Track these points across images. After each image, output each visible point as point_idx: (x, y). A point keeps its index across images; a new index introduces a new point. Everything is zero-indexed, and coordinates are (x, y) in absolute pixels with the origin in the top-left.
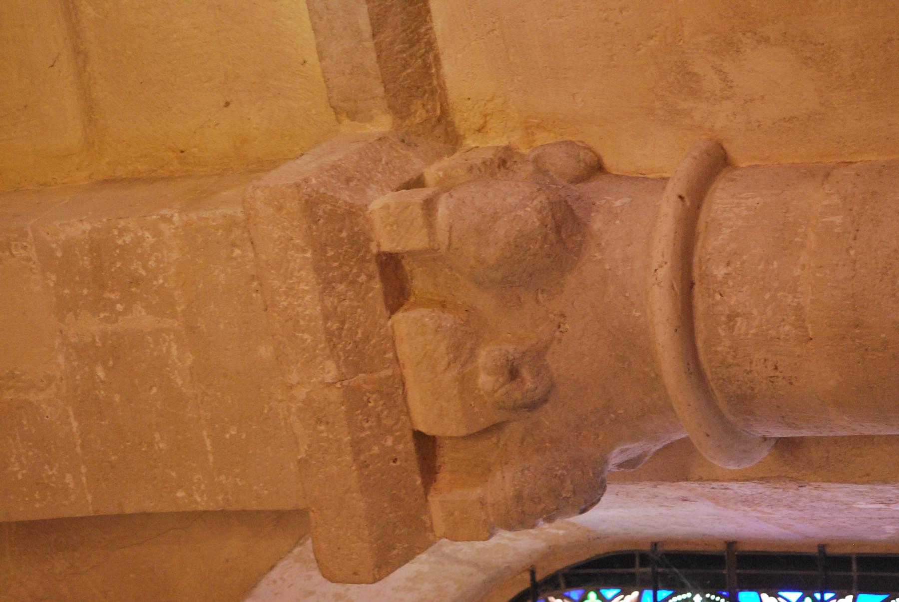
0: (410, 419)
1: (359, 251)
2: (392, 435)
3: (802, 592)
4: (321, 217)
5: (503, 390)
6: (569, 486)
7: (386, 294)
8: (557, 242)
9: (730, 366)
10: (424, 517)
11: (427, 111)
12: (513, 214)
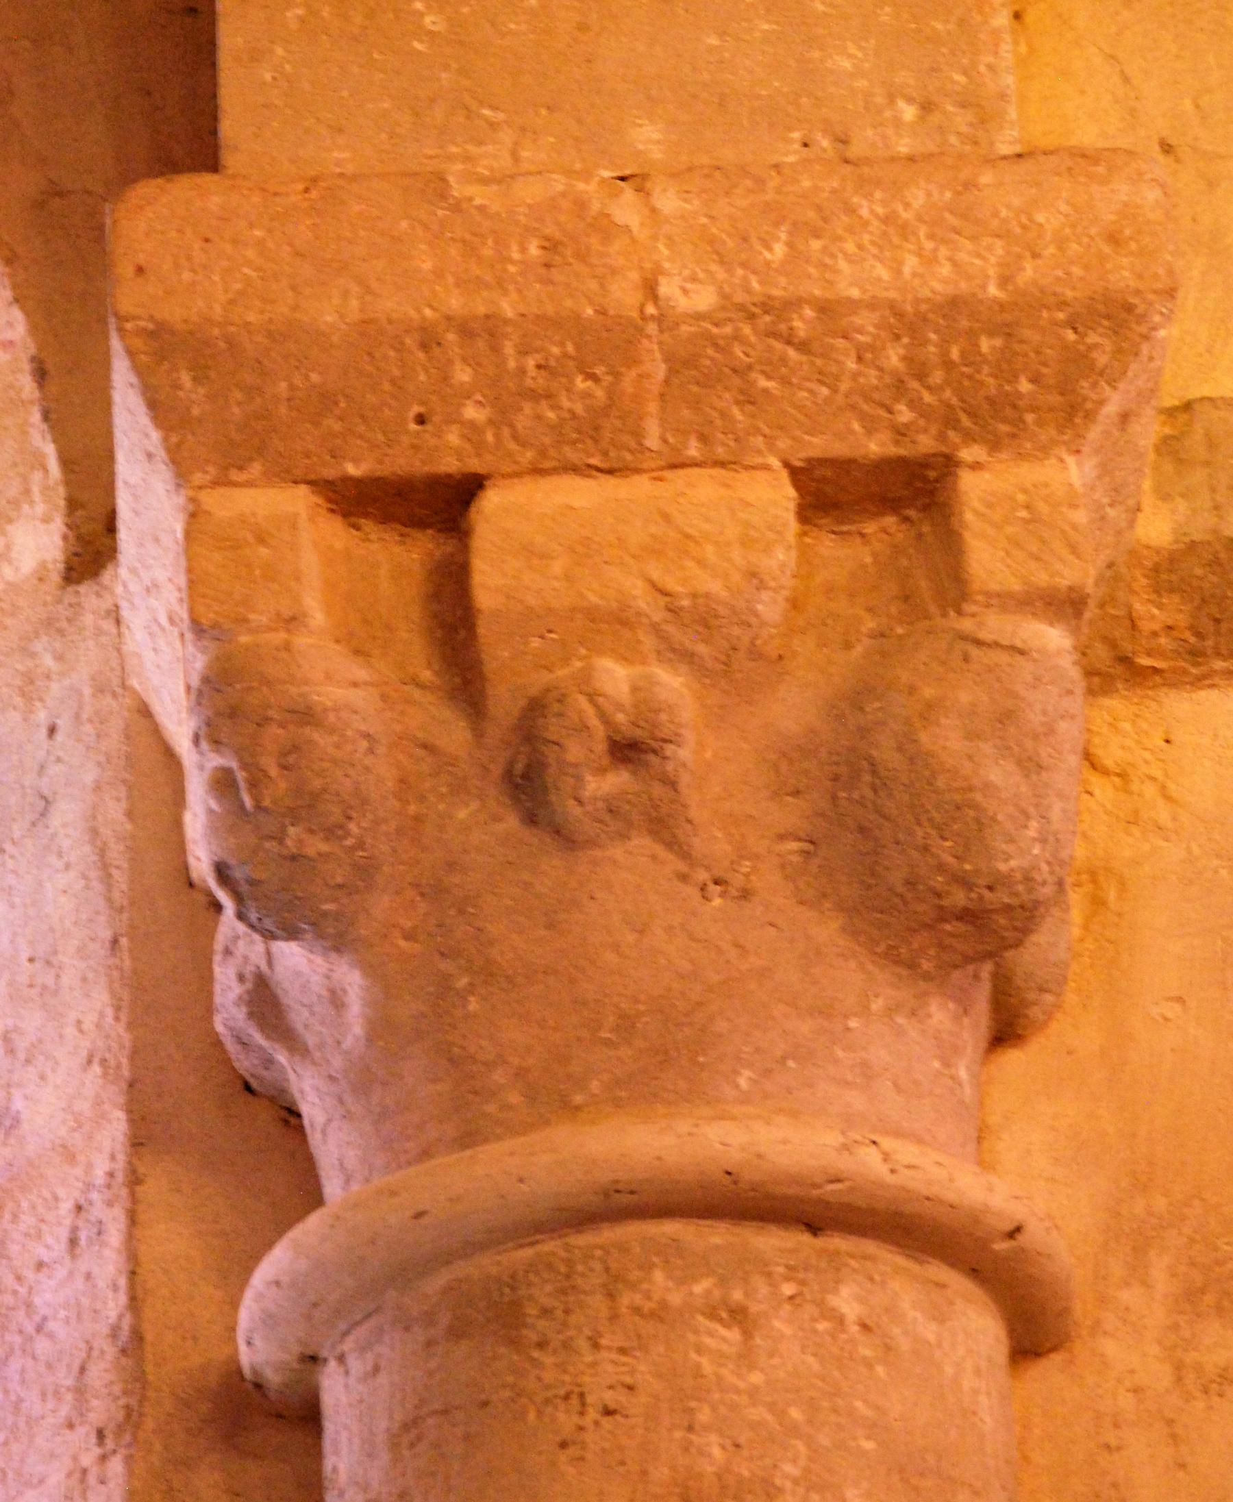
0: (518, 475)
1: (972, 414)
2: (491, 422)
4: (1083, 336)
5: (594, 722)
6: (316, 846)
7: (844, 465)
8: (941, 908)
9: (611, 1296)
10: (256, 469)
11: (1155, 634)
12: (1032, 810)
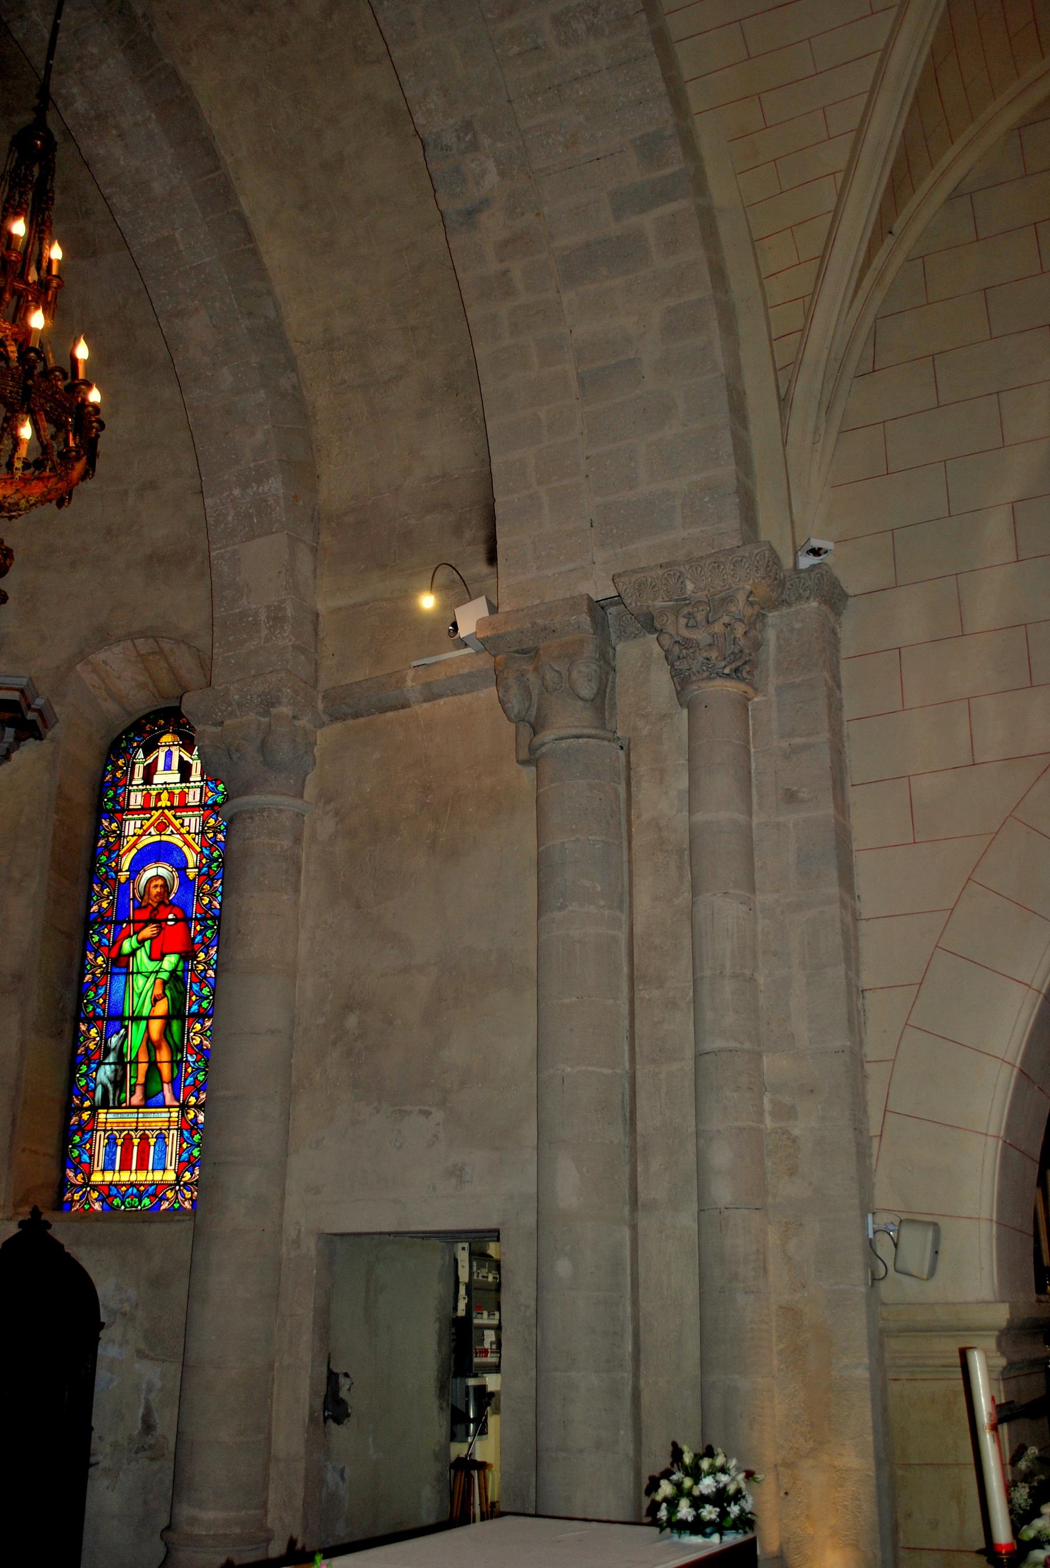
3: (47, 1232)
